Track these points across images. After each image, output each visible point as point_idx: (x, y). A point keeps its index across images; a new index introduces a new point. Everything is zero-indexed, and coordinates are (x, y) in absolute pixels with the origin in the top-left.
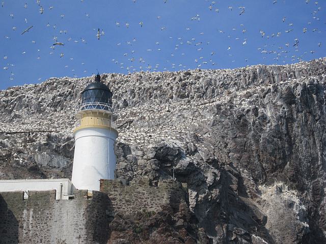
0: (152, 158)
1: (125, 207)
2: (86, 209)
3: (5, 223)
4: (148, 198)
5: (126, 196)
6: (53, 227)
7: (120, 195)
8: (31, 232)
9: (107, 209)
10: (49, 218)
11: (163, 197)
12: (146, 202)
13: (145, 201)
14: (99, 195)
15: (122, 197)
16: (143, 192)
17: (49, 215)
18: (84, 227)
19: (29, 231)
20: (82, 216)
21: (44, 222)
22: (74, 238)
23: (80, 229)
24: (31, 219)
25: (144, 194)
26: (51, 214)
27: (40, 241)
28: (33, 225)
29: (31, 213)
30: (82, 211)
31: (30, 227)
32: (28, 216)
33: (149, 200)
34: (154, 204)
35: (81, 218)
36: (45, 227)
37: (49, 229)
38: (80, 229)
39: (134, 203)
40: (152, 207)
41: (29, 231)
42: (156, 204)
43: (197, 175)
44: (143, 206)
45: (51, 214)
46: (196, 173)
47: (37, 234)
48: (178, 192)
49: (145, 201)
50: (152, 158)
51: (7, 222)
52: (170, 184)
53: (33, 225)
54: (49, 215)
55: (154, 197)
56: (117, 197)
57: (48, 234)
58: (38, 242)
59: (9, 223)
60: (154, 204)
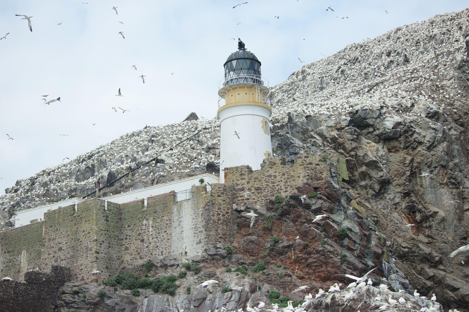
0: (347, 126)
1: (255, 197)
2: (204, 208)
3: (126, 239)
4: (281, 181)
5: (255, 183)
6: (173, 234)
7: (248, 183)
8: (152, 245)
9: (234, 203)
10: (169, 224)
11: (299, 177)
12: (279, 187)
13: (278, 185)
14: (219, 188)
15: (250, 185)
16: (275, 174)
17: (168, 222)
18: (202, 229)
19: (150, 243)
20: (200, 216)
21: (163, 231)
23: (200, 232)
24: (151, 229)
25: (275, 177)
26: (170, 220)
27: (160, 254)
28: (154, 236)
29: (151, 222)
30: (200, 211)
31: (151, 238)
33: (282, 184)
34: (289, 187)
36: (165, 236)
37: (169, 237)
38: (200, 232)
39: (265, 189)
40: (286, 191)
41: (150, 243)
42: (291, 187)
43: (411, 135)
44: (276, 192)
45: (170, 220)
46: (410, 133)
47: (157, 246)
48: (317, 166)
49: (278, 185)
50: (347, 126)
51: (128, 237)
52: (306, 159)
53: (154, 236)
54: (168, 222)
55: (288, 178)
56: (245, 186)
57: (168, 244)
58: (159, 255)
59: (131, 238)
60: (289, 187)
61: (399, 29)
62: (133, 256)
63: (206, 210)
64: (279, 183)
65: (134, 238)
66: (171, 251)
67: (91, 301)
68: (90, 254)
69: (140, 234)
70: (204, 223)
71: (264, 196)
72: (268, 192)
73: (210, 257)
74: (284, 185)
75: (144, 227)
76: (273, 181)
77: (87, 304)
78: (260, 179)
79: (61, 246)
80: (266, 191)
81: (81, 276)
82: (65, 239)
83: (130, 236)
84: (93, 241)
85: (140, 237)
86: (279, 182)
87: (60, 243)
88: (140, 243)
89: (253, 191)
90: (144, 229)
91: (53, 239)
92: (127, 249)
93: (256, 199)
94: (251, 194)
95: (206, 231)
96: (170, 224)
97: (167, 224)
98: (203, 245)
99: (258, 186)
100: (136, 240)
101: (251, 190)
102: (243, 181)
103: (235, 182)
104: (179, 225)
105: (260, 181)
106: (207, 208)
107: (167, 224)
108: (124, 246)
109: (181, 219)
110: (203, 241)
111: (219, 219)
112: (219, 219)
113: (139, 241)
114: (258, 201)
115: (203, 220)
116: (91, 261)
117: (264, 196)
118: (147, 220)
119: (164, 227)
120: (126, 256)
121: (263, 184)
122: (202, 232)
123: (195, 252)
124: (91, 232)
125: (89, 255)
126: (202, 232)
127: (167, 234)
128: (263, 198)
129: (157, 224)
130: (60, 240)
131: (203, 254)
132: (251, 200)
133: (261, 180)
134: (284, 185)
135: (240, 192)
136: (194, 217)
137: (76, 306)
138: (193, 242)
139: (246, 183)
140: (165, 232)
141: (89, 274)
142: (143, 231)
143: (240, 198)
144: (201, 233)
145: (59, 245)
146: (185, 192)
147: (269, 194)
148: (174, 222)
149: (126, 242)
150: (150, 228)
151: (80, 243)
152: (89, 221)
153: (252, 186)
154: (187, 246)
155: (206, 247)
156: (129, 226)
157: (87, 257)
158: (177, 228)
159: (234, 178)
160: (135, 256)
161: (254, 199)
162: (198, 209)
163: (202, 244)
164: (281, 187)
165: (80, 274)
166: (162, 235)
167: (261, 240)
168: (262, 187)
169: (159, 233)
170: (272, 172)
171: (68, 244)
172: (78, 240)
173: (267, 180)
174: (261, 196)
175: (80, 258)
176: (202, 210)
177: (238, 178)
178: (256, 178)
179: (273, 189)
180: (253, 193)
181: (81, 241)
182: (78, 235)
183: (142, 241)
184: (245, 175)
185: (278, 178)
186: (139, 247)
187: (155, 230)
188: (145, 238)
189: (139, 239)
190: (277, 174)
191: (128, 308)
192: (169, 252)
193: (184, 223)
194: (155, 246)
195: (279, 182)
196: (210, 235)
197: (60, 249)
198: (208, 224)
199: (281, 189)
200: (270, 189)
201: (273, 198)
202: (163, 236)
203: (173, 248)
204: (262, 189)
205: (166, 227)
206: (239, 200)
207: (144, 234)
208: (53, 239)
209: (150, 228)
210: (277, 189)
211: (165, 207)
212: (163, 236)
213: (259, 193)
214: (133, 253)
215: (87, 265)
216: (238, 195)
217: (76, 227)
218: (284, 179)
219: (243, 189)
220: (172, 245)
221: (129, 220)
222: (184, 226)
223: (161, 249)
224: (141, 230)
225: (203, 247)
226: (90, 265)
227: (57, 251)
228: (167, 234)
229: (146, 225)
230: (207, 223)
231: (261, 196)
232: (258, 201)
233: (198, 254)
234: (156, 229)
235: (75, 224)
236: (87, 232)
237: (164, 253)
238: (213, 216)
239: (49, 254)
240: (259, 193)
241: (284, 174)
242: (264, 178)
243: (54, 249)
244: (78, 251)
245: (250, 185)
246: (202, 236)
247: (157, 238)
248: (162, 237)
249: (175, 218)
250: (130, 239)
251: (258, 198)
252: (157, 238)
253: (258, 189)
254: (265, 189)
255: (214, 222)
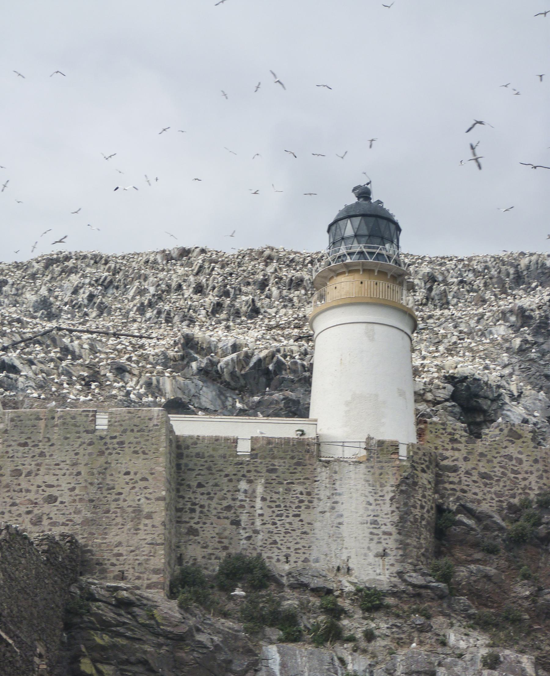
0: (446, 400)
2: (398, 486)
4: (531, 473)
5: (481, 464)
6: (317, 525)
7: (466, 459)
8: (260, 537)
12: (526, 483)
13: (525, 479)
16: (520, 456)
19: (256, 532)
20: (388, 502)
21: (291, 513)
22: (371, 555)
23: (385, 533)
24: (259, 503)
25: (520, 462)
26: (309, 494)
27: (283, 559)
28: (266, 518)
29: (260, 489)
30: (388, 491)
31: (258, 522)
32: (252, 496)
33: (533, 478)
35: (387, 508)
36: (296, 524)
37: (306, 528)
41: (256, 532)
47: (275, 542)
49: (525, 479)
50: (446, 400)
51: (197, 507)
53: (266, 518)
54: (304, 497)
56: (459, 464)
57: (303, 543)
58: (278, 560)
59: (205, 510)
61: (478, 256)
62: (210, 551)
63: (402, 492)
64: (526, 476)
65: (214, 512)
66: (312, 558)
67: (169, 629)
68: (146, 525)
69: (229, 508)
70: (396, 518)
71: (495, 493)
72: (505, 486)
73: (410, 588)
74: (537, 482)
75: (241, 496)
76: (516, 468)
77: (157, 635)
78: (489, 457)
79: (54, 492)
80: (501, 484)
81: (118, 568)
82: (68, 478)
83: (202, 506)
84: (158, 499)
85: (230, 514)
86: (526, 472)
87: (52, 486)
88: (229, 526)
89: (475, 478)
90: (241, 501)
91: (29, 474)
92: (193, 532)
93: (480, 495)
94: (471, 483)
95: (399, 533)
96: (310, 502)
97: (302, 501)
98: (392, 562)
99: (486, 471)
100: (219, 518)
101: (471, 474)
102: (457, 454)
103: (440, 451)
104: (333, 508)
105: (489, 461)
106: (404, 488)
107: (302, 501)
108: (188, 525)
109: (337, 498)
110: (394, 553)
111: (422, 518)
112: (422, 518)
113: (228, 522)
114: (484, 499)
115: (393, 512)
116: (149, 540)
117: (495, 493)
118: (250, 482)
119: (294, 506)
120: (190, 547)
121: (495, 469)
122: (390, 534)
123: (371, 572)
124: (150, 477)
125: (141, 526)
126: (390, 534)
127: (301, 521)
128: (494, 496)
129: (275, 497)
130: (51, 480)
131: (393, 579)
132: (469, 495)
133: (492, 461)
134: (537, 482)
135: (450, 474)
136: (371, 500)
137: (129, 634)
138: (366, 551)
139: (461, 458)
140: (295, 516)
141: (142, 569)
142: (238, 503)
143: (447, 485)
144: (386, 537)
145: (48, 489)
146: (341, 444)
147: (507, 493)
148: (319, 499)
149: (192, 518)
150: (258, 500)
151: (114, 497)
152: (144, 453)
153: (474, 468)
154: (353, 556)
155: (398, 568)
156: (200, 485)
157: (138, 529)
158: (328, 514)
159: (438, 442)
160: (216, 552)
161: (475, 494)
162: (382, 485)
163: (390, 559)
164: (530, 483)
165: (113, 565)
166: (288, 520)
167: (503, 577)
168: (492, 474)
169: (281, 515)
170: (512, 450)
171: (77, 491)
172: (109, 489)
173: (503, 464)
174: (489, 492)
175: (114, 530)
176: (393, 491)
177: (447, 446)
178: (482, 455)
179: (515, 482)
180: (475, 482)
181: (120, 494)
182: (109, 478)
183: (236, 523)
184: (460, 442)
185: (526, 466)
186: (227, 533)
187: (270, 507)
188: (244, 518)
189: (227, 518)
190: (523, 457)
191: (240, 663)
192: (306, 560)
193: (344, 506)
194: (270, 541)
195: (526, 472)
196: (408, 544)
197: (52, 499)
198: (406, 521)
199: (530, 489)
200: (508, 483)
201: (516, 501)
202: (290, 523)
203: (315, 554)
204: (492, 479)
205: (299, 507)
206: (446, 489)
207: (241, 510)
208: (29, 474)
209: (258, 500)
210: (522, 486)
211: (298, 464)
212: (290, 523)
213: (486, 485)
214: (211, 544)
215: (138, 548)
216: (446, 479)
217: (102, 460)
218: (538, 470)
219: (455, 469)
220: (314, 547)
221: (202, 473)
222: (346, 514)
223: (284, 549)
224: (234, 499)
225: (392, 565)
226: (147, 549)
227: (40, 501)
228: (301, 521)
229: (246, 491)
230: (402, 519)
231: (489, 492)
232: (484, 499)
233: (378, 577)
234: (273, 505)
235: (101, 453)
236: (139, 476)
237: (292, 559)
238: (415, 507)
239: (14, 504)
240: (486, 485)
241: (536, 461)
242: (499, 459)
243: (31, 496)
244: (108, 511)
245: (469, 465)
246: (391, 543)
247: (274, 524)
248: (287, 526)
249: (324, 494)
250: (201, 512)
251: (484, 494)
252: (274, 524)
253: (484, 476)
254: (498, 481)
255: (416, 520)
